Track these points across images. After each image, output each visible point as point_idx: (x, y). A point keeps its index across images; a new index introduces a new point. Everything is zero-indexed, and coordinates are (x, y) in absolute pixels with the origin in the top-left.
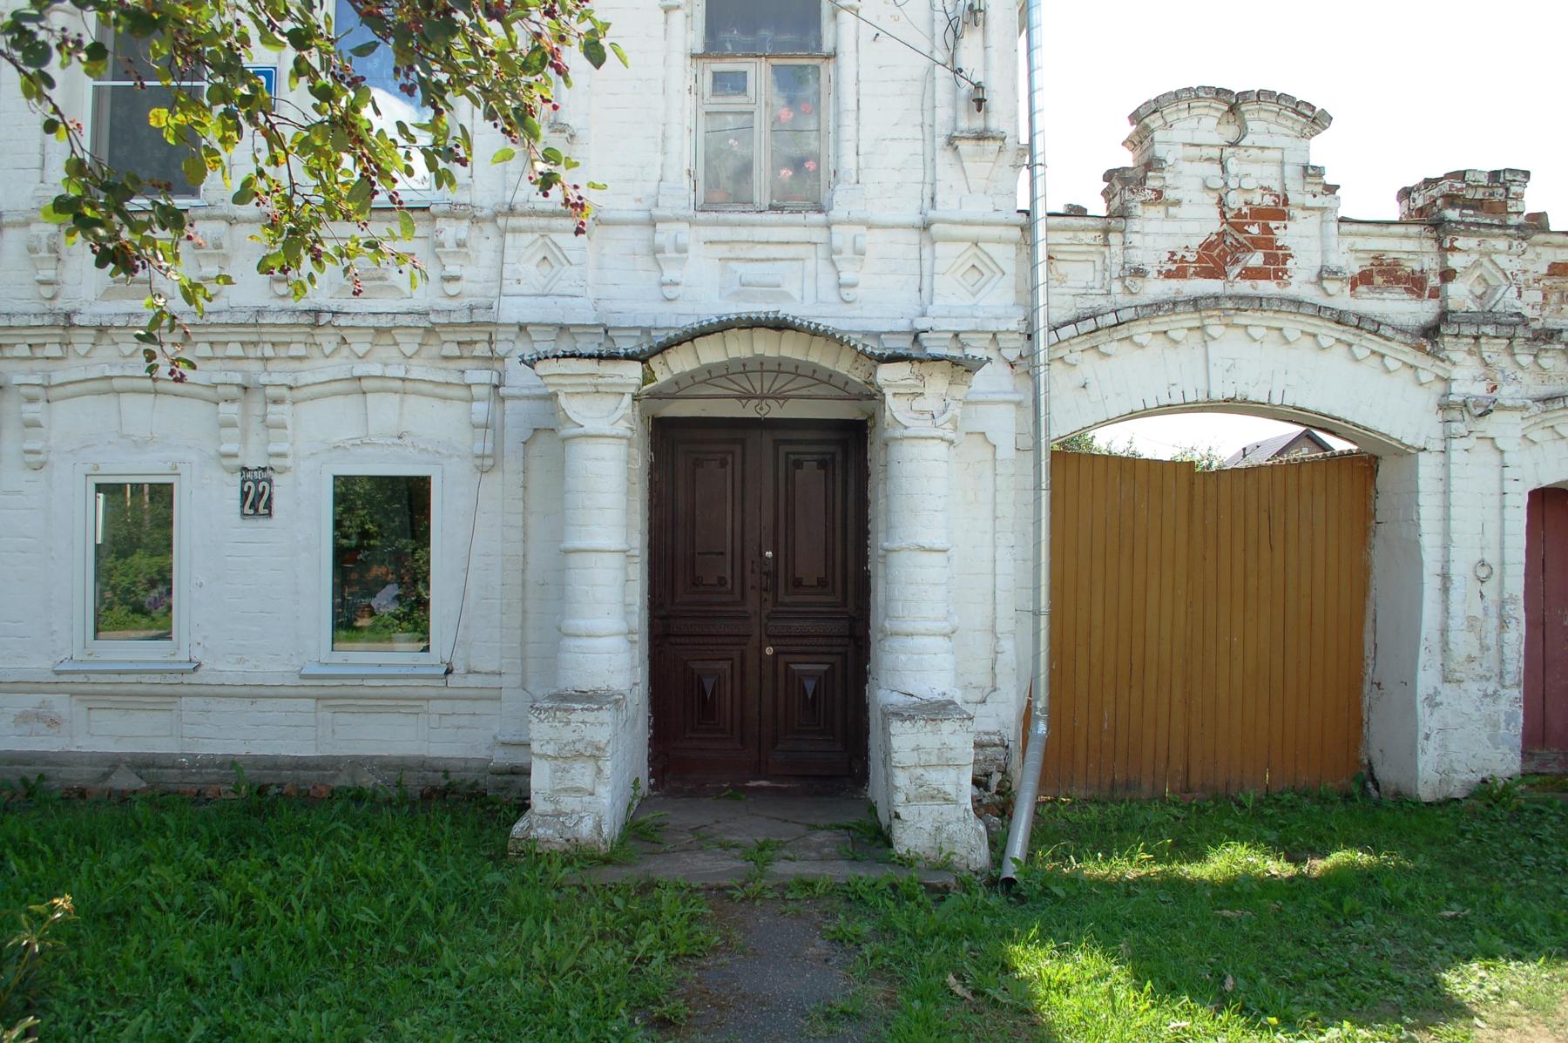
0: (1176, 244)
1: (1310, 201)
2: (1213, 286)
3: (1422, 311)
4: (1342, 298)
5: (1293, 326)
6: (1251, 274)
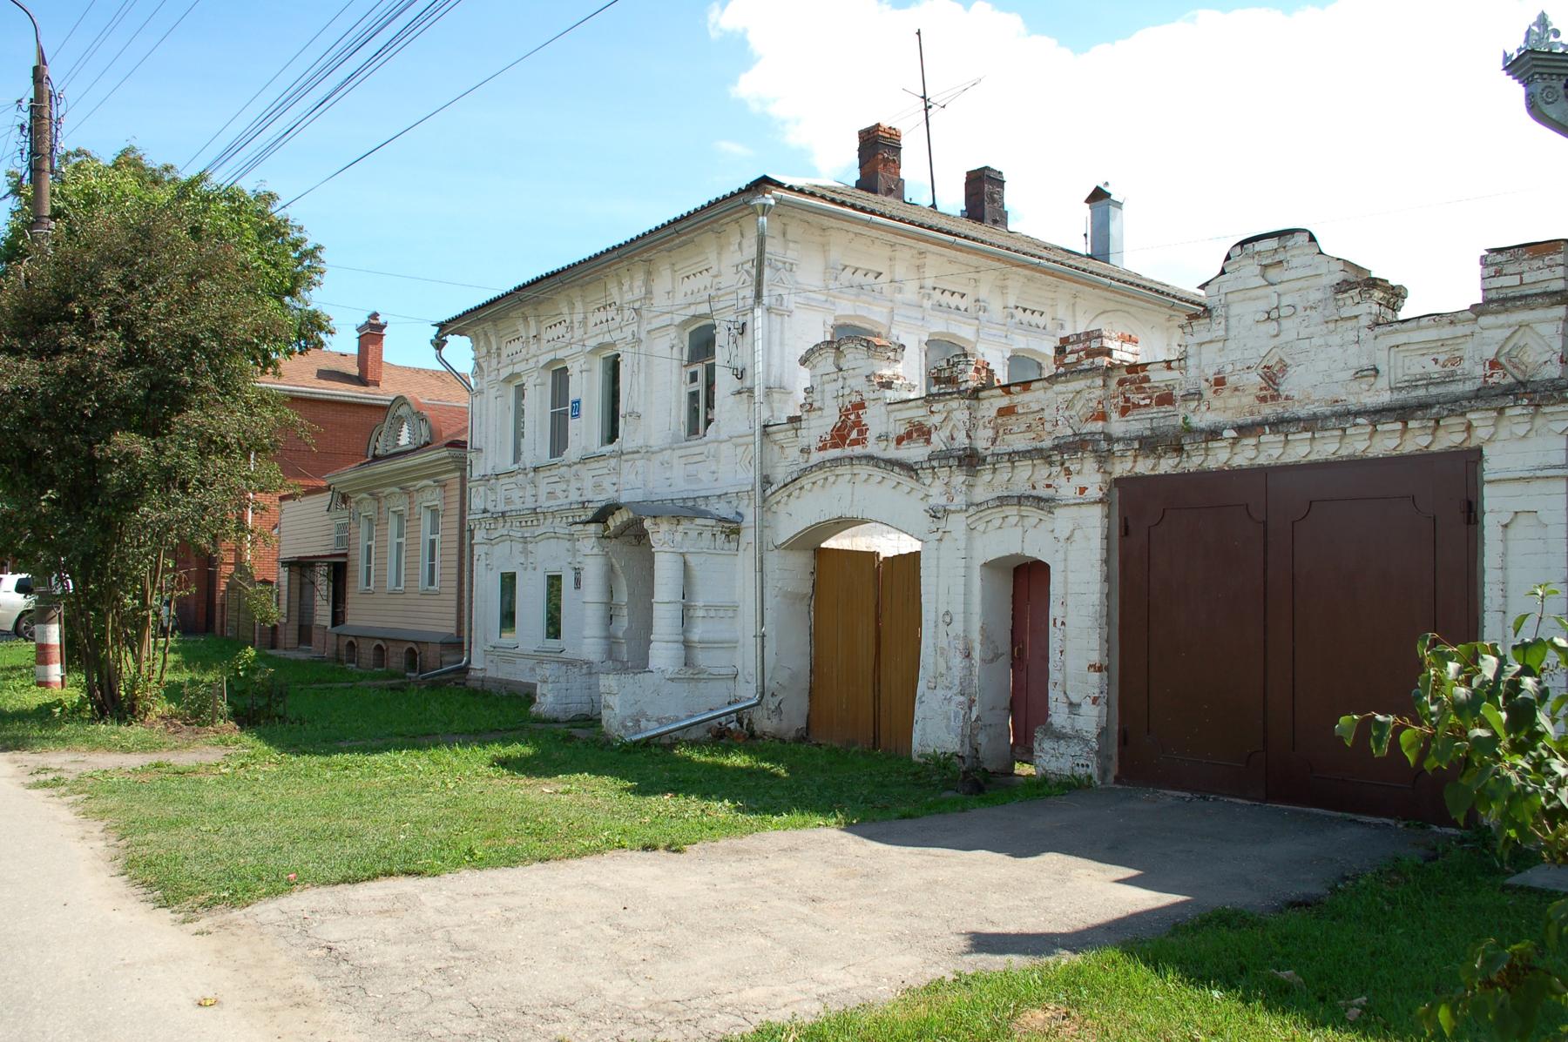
0: (821, 432)
1: (873, 396)
2: (836, 453)
3: (929, 449)
4: (893, 453)
5: (863, 470)
6: (855, 442)
